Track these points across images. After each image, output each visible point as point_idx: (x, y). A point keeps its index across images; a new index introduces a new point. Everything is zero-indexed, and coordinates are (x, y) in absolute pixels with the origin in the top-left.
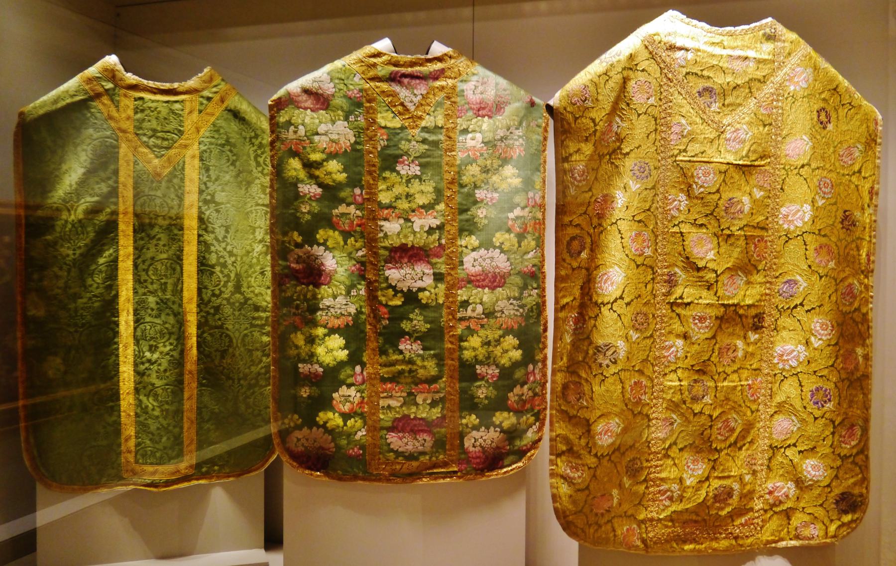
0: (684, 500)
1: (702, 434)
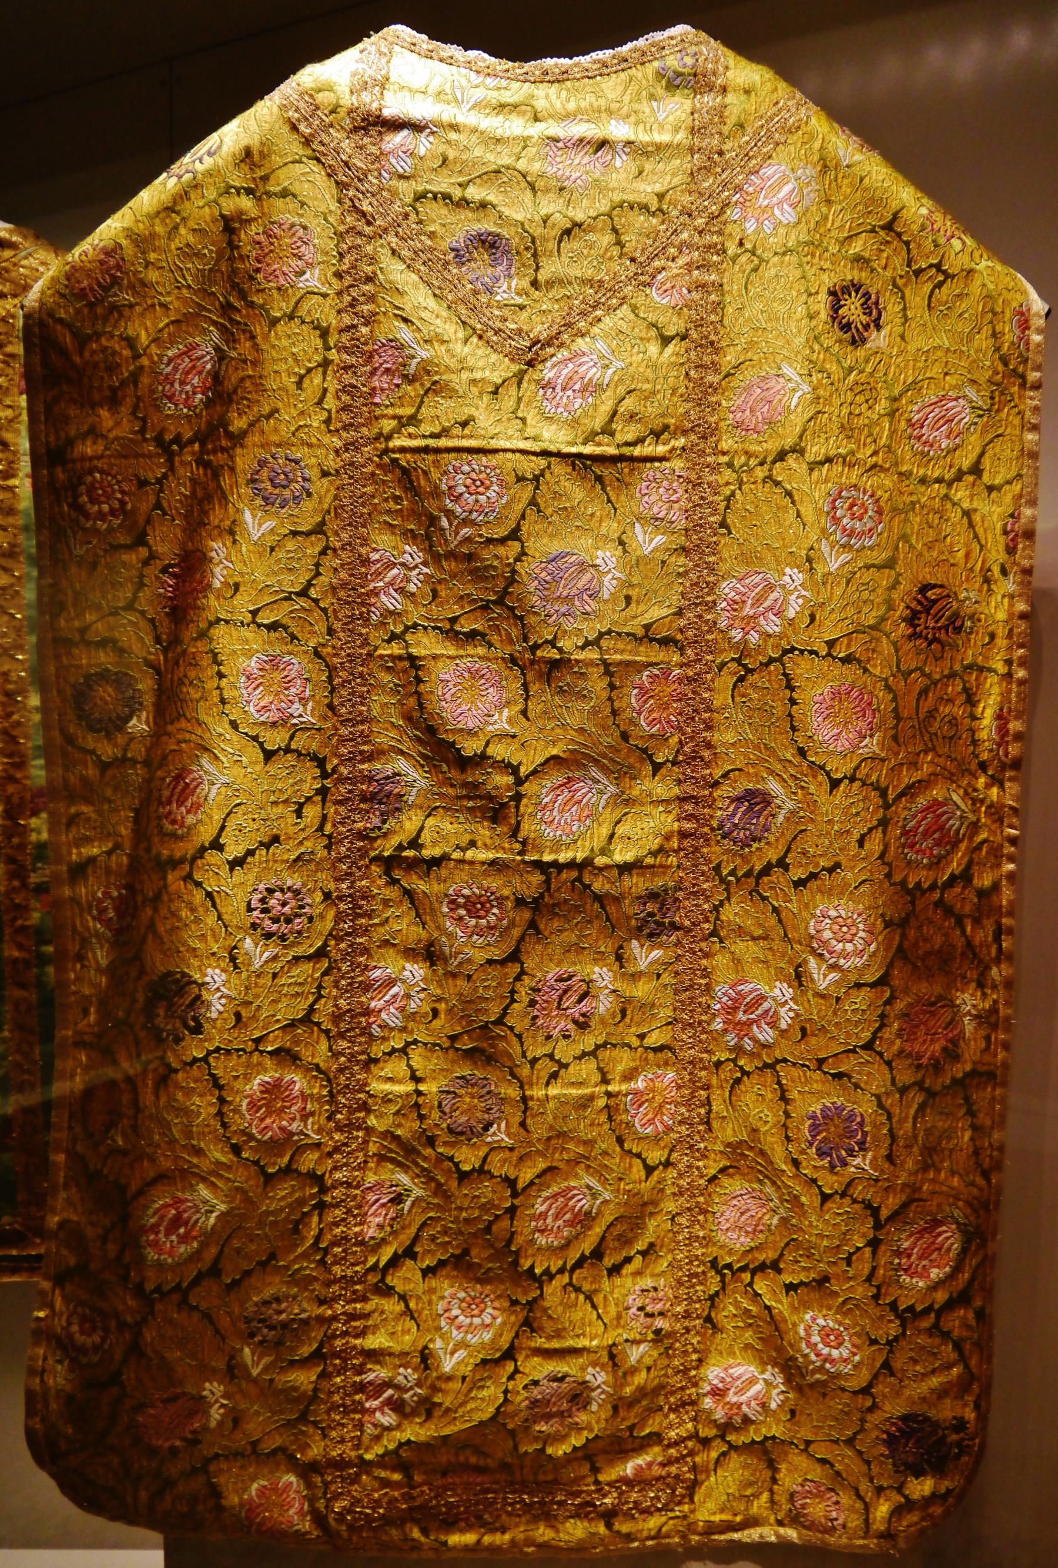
0: (437, 1413)
1: (488, 1229)
